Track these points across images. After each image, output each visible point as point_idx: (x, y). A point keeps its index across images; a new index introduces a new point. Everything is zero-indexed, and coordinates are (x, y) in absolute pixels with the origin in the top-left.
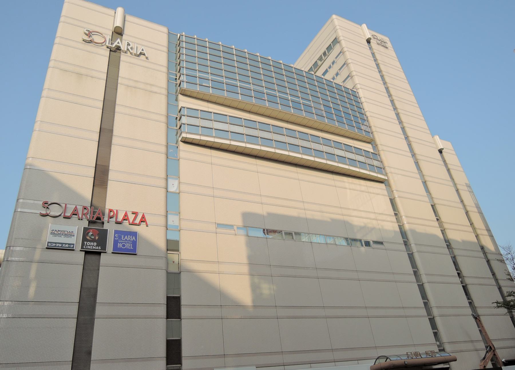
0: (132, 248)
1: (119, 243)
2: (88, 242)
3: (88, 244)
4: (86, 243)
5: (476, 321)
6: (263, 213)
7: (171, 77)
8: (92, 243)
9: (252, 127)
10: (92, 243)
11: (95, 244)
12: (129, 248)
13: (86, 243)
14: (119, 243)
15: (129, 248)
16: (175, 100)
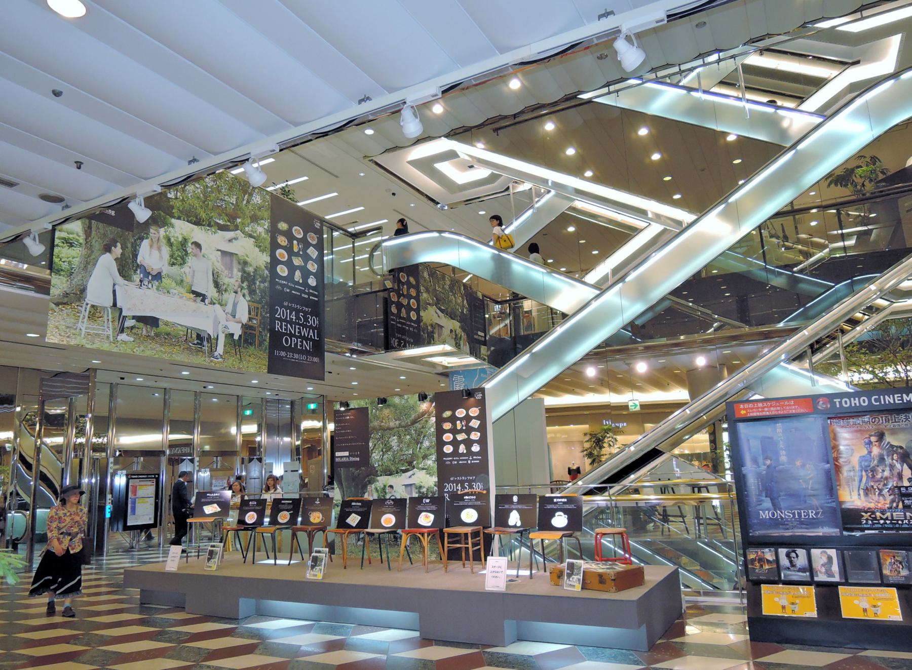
0: (835, 400)
1: (900, 395)
2: (844, 400)
3: (846, 403)
4: (840, 403)
5: (45, 372)
6: (344, 300)
7: (31, 337)
8: (855, 400)
9: (418, 231)
10: (855, 400)
11: (864, 401)
12: (897, 402)
13: (840, 403)
14: (900, 395)
15: (897, 402)
16: (536, 244)
